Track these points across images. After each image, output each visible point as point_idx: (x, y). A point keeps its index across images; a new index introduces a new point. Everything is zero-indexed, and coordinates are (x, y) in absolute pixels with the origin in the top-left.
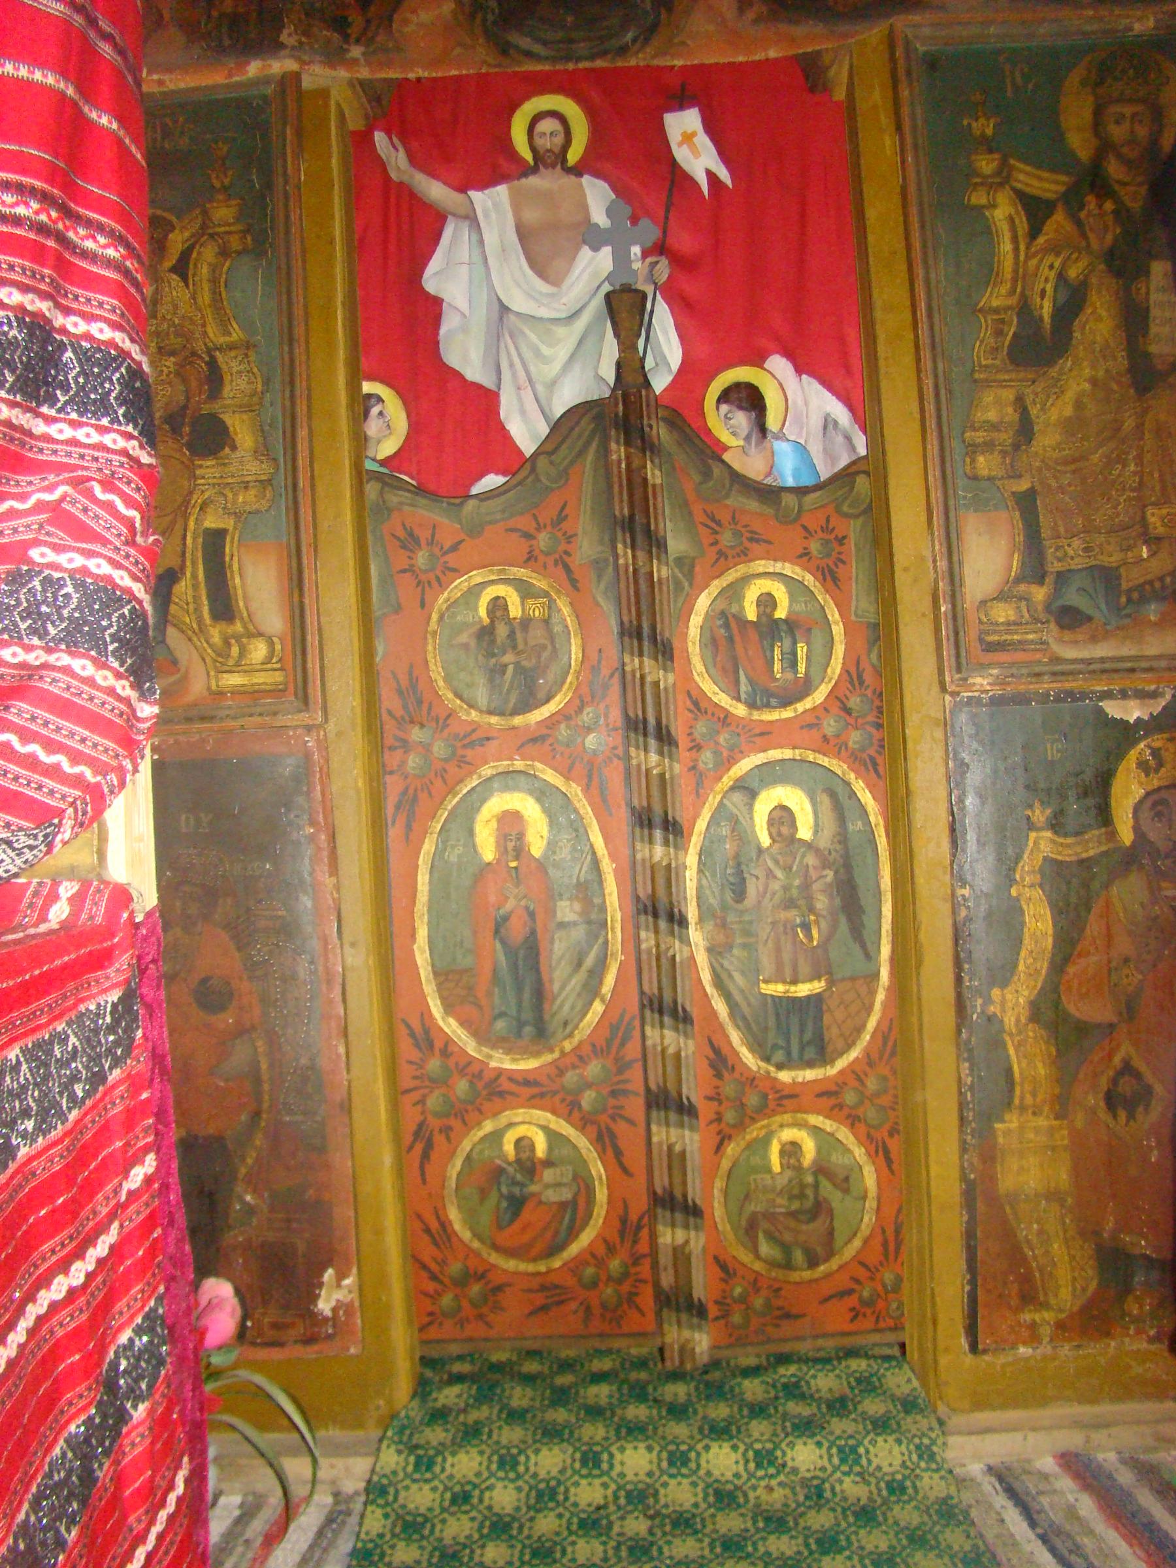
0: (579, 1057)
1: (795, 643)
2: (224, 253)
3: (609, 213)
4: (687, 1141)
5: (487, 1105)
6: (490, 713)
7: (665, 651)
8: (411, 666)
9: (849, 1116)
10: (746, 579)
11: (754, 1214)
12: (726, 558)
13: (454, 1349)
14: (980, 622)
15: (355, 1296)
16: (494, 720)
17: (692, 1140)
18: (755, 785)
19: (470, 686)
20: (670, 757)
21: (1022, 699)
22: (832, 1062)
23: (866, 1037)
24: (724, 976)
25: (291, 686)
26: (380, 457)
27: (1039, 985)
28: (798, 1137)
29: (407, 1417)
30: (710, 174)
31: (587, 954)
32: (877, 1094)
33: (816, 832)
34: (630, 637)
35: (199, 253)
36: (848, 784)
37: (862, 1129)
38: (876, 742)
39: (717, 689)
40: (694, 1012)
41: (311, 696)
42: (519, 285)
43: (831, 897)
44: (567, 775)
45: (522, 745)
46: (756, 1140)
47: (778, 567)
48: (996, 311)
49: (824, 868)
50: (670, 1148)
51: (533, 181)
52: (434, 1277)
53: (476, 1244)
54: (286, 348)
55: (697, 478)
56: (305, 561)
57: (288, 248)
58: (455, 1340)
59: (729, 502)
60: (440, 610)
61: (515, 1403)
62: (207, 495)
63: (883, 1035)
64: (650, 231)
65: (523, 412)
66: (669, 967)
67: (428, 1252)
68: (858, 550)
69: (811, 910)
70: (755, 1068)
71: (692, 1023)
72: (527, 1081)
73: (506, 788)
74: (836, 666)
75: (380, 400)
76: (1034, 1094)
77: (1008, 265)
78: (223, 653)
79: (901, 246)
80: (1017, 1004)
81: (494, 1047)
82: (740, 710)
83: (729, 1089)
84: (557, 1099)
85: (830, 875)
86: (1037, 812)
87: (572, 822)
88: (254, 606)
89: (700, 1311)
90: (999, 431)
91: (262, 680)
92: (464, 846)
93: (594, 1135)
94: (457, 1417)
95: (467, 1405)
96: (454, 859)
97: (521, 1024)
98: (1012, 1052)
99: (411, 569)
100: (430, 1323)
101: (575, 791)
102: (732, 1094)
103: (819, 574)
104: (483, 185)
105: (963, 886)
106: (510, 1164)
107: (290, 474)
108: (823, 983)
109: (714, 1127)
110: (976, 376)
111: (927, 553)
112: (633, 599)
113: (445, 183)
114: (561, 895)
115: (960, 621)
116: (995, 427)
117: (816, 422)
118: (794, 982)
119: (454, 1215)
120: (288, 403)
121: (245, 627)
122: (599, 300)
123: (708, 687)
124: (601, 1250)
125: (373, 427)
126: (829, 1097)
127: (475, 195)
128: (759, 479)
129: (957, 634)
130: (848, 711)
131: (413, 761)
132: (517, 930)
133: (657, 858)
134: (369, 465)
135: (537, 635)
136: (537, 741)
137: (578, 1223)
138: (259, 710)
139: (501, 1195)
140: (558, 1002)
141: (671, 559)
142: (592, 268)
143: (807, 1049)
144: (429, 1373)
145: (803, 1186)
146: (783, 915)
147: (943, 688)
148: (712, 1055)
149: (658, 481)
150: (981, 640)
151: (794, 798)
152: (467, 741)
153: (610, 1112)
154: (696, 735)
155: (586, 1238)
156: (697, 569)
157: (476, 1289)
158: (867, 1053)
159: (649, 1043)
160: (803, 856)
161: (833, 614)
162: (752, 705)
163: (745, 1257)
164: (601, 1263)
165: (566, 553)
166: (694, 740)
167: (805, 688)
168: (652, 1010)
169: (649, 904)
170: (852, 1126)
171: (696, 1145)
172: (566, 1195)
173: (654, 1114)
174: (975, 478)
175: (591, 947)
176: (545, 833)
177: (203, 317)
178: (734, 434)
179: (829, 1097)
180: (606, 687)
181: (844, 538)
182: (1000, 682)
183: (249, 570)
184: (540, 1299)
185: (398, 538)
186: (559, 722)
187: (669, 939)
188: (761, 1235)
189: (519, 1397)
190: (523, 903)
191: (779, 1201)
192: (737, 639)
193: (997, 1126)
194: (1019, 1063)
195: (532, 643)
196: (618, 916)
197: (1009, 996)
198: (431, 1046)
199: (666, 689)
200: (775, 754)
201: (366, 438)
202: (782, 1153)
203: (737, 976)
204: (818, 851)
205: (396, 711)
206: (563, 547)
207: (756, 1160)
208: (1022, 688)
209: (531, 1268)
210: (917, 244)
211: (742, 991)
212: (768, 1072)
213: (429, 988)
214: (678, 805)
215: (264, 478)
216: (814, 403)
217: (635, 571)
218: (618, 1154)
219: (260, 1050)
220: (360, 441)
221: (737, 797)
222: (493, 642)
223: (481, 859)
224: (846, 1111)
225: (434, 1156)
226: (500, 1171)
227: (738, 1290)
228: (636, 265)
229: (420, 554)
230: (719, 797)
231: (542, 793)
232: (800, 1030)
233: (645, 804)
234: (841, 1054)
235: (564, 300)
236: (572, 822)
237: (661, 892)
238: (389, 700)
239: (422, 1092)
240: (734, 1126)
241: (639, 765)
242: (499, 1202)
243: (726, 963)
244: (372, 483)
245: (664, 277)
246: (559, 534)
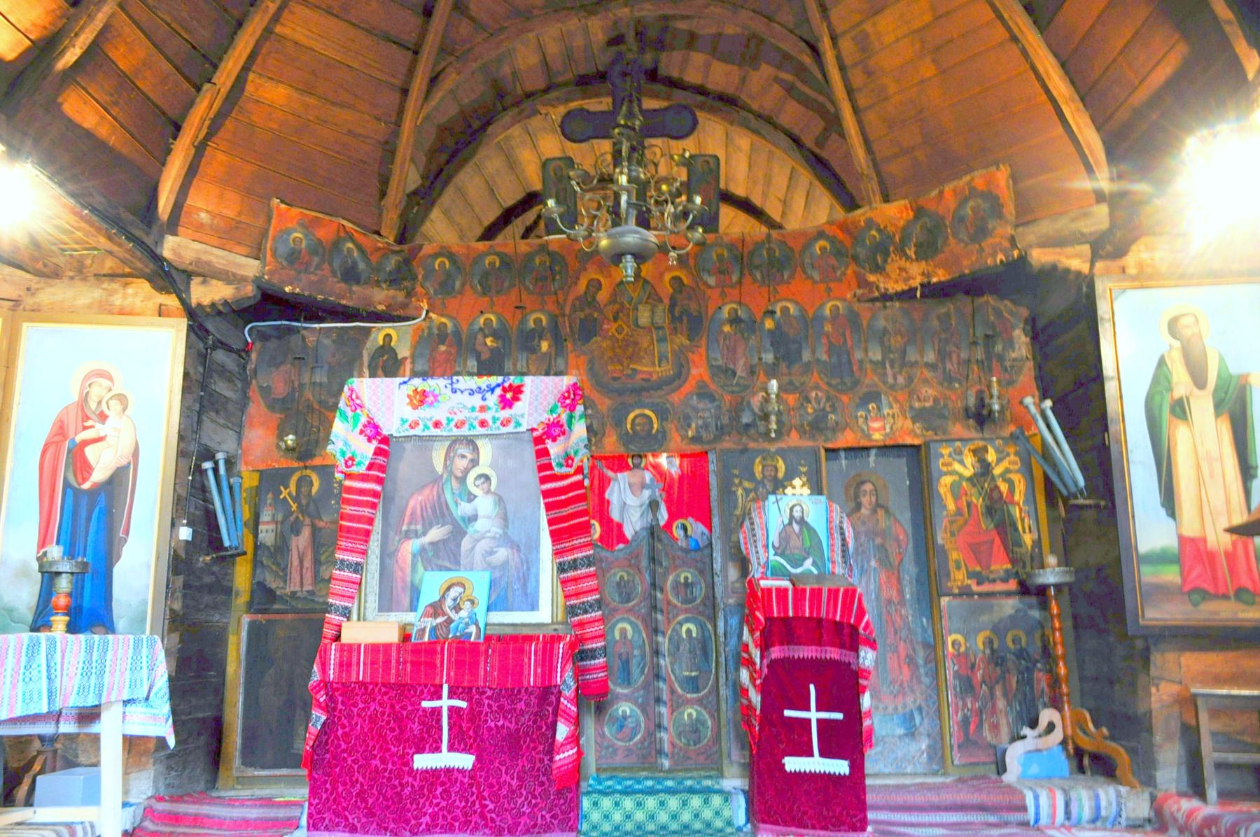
67: (599, 740)
72: (626, 695)
101: (639, 623)
126: (700, 702)
132: (624, 657)
136: (630, 610)
155: (639, 737)
163: (677, 741)
167: (694, 600)
231: (631, 623)
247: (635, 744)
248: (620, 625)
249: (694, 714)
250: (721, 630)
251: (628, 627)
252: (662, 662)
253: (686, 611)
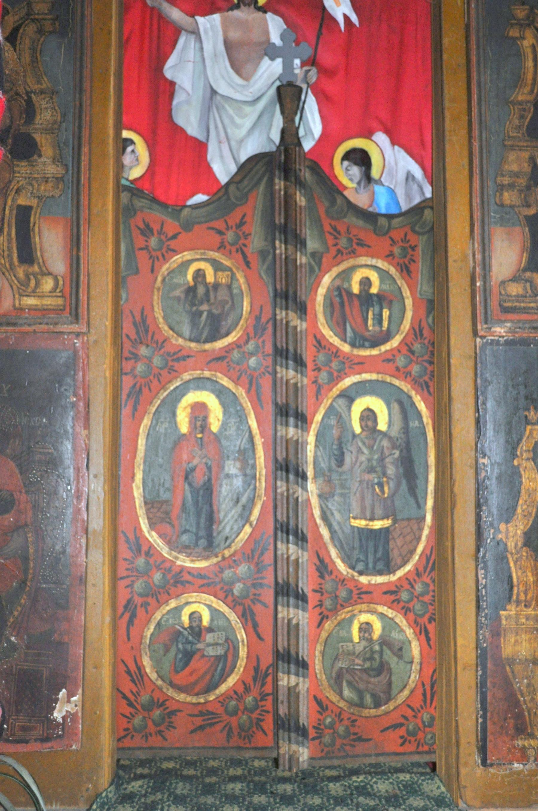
0: (232, 562)
2: (40, 31)
3: (282, 37)
4: (300, 618)
5: (172, 590)
6: (191, 340)
7: (302, 309)
8: (143, 309)
10: (354, 268)
12: (342, 254)
13: (142, 755)
14: (501, 294)
15: (79, 708)
16: (193, 345)
17: (303, 617)
18: (353, 394)
19: (178, 323)
20: (302, 374)
21: (524, 342)
23: (416, 557)
24: (328, 513)
25: (68, 309)
26: (131, 178)
27: (531, 522)
28: (370, 620)
29: (107, 796)
30: (346, 17)
31: (243, 495)
32: (422, 594)
34: (281, 298)
35: (24, 30)
36: (410, 397)
38: (428, 372)
39: (331, 333)
40: (309, 536)
41: (80, 314)
42: (223, 77)
43: (397, 468)
44: (236, 382)
45: (210, 362)
46: (343, 620)
47: (374, 262)
48: (520, 103)
50: (289, 621)
51: (236, 13)
52: (130, 704)
53: (159, 682)
54: (77, 95)
55: (327, 204)
56: (82, 229)
57: (82, 32)
58: (140, 748)
59: (346, 220)
60: (163, 275)
61: (179, 792)
62: (21, 183)
63: (426, 557)
64: (307, 50)
65: (222, 157)
66: (294, 505)
67: (127, 687)
68: (423, 254)
69: (384, 474)
70: (345, 573)
71: (307, 542)
72: (200, 574)
73: (198, 388)
74: (407, 325)
75: (132, 142)
76: (526, 594)
77: (530, 76)
78: (25, 283)
79: (463, 61)
80: (516, 534)
81: (180, 552)
82: (346, 348)
83: (328, 586)
85: (397, 453)
86: (532, 413)
87: (237, 411)
88: (47, 255)
89: (303, 732)
90: (518, 177)
91: (49, 303)
92: (170, 422)
93: (240, 614)
94: (139, 799)
95: (146, 792)
98: (512, 565)
99: (146, 248)
100: (125, 736)
101: (241, 392)
102: (329, 589)
103: (399, 268)
104: (205, 13)
105: (484, 457)
107: (75, 175)
108: (390, 521)
109: (318, 610)
110: (506, 143)
111: (470, 252)
112: (284, 275)
113: (182, 11)
115: (488, 292)
116: (516, 175)
117: (401, 176)
118: (372, 519)
119: (146, 662)
120: (76, 130)
121: (40, 268)
122: (273, 91)
124: (241, 689)
125: (127, 159)
126: (391, 595)
127: (200, 19)
128: (365, 207)
129: (486, 300)
130: (412, 352)
131: (140, 368)
132: (199, 479)
133: (290, 435)
134: (123, 182)
135: (222, 294)
136: (220, 359)
137: (227, 669)
138: (46, 320)
139: (178, 650)
140: (223, 524)
141: (309, 251)
142: (269, 71)
143: (378, 564)
144: (121, 773)
145: (373, 652)
146: (367, 477)
147: (475, 333)
148: (318, 563)
149: (303, 203)
150: (500, 305)
151: (377, 405)
152: (175, 357)
153: (252, 597)
155: (231, 681)
156: (324, 260)
159: (279, 552)
160: (381, 440)
161: (406, 293)
162: (353, 345)
163: (334, 698)
164: (240, 699)
165: (245, 245)
166: (316, 365)
167: (387, 337)
168: (282, 531)
169: (284, 464)
171: (306, 621)
172: (220, 651)
173: (280, 599)
174: (502, 205)
175: (245, 491)
177: (24, 71)
178: (351, 180)
179: (391, 595)
180: (264, 329)
181: (416, 246)
182: (511, 331)
183: (46, 233)
184: (199, 721)
186: (233, 349)
187: (296, 486)
189: (181, 788)
190: (204, 460)
191: (357, 661)
192: (346, 303)
193: (502, 613)
196: (264, 472)
197: (511, 529)
198: (139, 551)
199: (301, 331)
200: (366, 376)
201: (123, 166)
202: (360, 629)
204: (390, 438)
205: (133, 334)
207: (343, 633)
208: (525, 335)
209: (194, 700)
210: (474, 59)
211: (339, 524)
212: (353, 576)
213: (141, 512)
214: (305, 404)
215: (59, 176)
216: (401, 163)
217: (286, 258)
218: (255, 626)
219: (30, 540)
220: (120, 167)
222: (195, 296)
223: (180, 431)
224: (402, 604)
225: (136, 621)
226: (180, 633)
228: (297, 71)
230: (330, 401)
231: (221, 393)
232: (375, 550)
233: (284, 401)
234: (399, 568)
235: (251, 90)
236: (237, 411)
237: (292, 457)
238: (128, 328)
239: (132, 579)
240: (330, 610)
241: (282, 378)
242: (176, 655)
244: (125, 193)
245: (314, 79)
246: (240, 233)
248: (192, 397)
249: (377, 627)
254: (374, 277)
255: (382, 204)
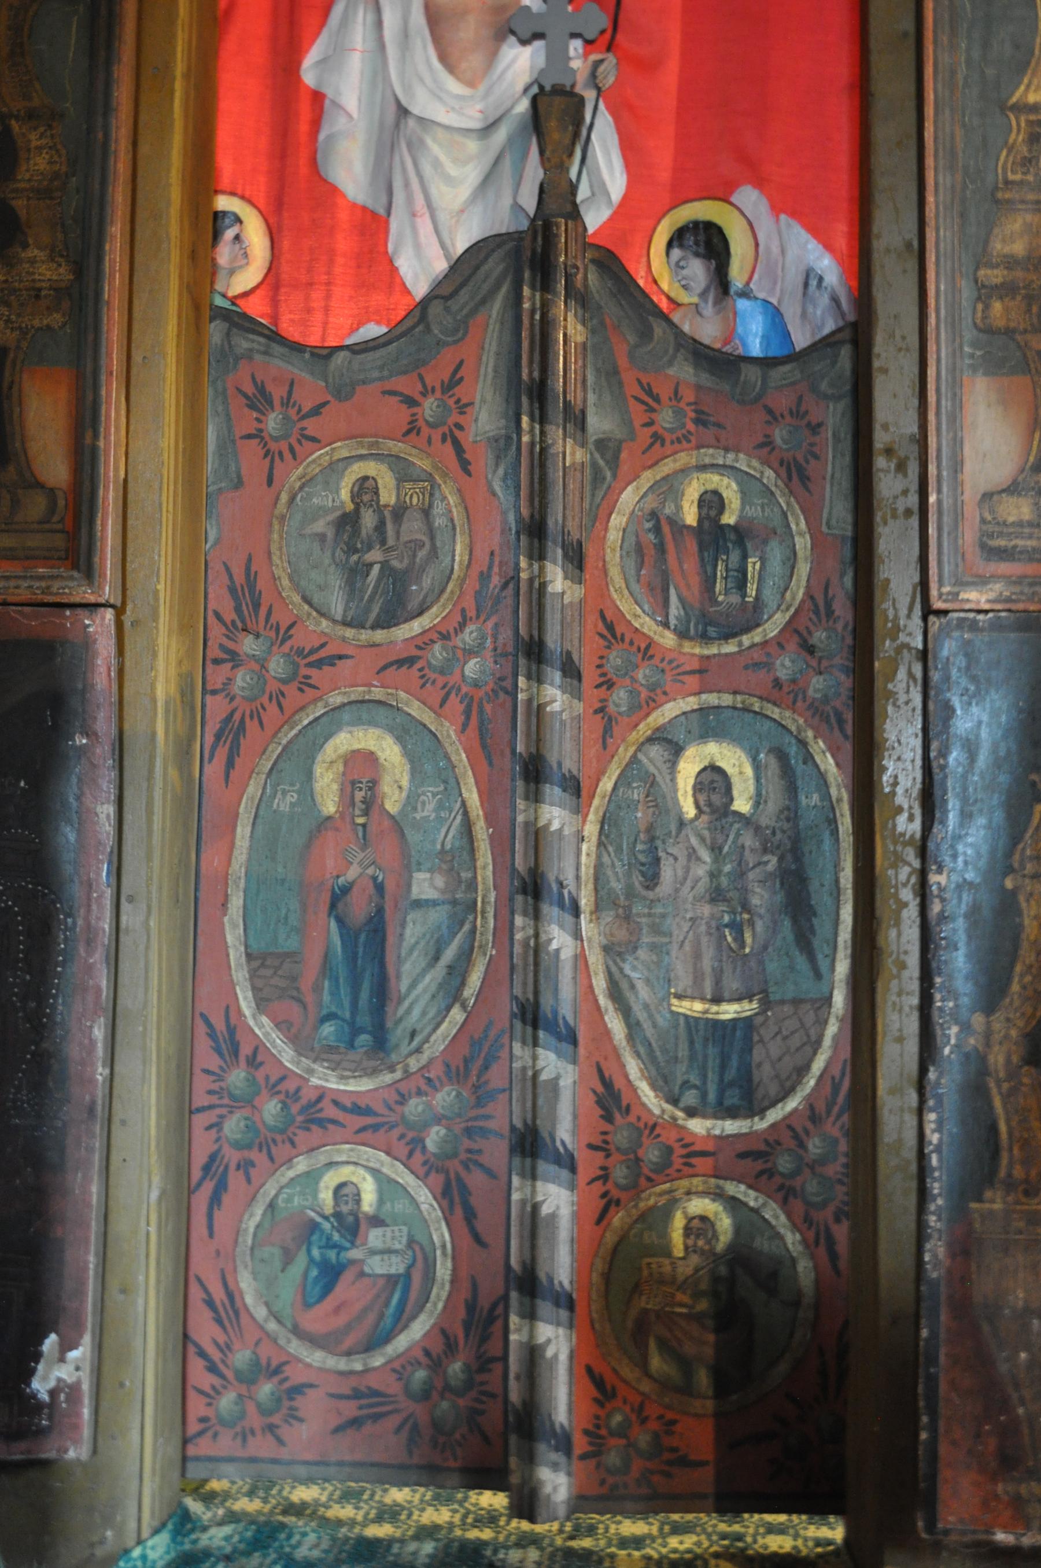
1: (745, 557)
5: (301, 1137)
9: (781, 1187)
11: (645, 1312)
16: (349, 633)
18: (680, 737)
22: (762, 1112)
24: (624, 985)
26: (230, 294)
33: (757, 804)
36: (803, 743)
37: (798, 1206)
44: (439, 708)
45: (384, 668)
49: (765, 851)
53: (272, 1326)
55: (632, 339)
59: (671, 371)
69: (746, 907)
70: (657, 1111)
73: (358, 722)
74: (798, 591)
75: (238, 220)
82: (668, 639)
83: (621, 1138)
84: (396, 1133)
85: (772, 862)
92: (299, 792)
93: (439, 1190)
96: (284, 808)
97: (356, 1030)
99: (258, 435)
101: (448, 732)
106: (326, 1218)
108: (755, 1005)
109: (598, 1188)
114: (419, 864)
117: (793, 278)
118: (717, 1000)
119: (246, 1284)
123: (626, 606)
125: (224, 254)
130: (810, 650)
132: (359, 908)
135: (413, 527)
137: (409, 1308)
139: (312, 1260)
140: (406, 1004)
148: (600, 1089)
151: (732, 759)
153: (463, 1156)
154: (608, 668)
155: (418, 1329)
156: (624, 455)
157: (266, 1389)
158: (810, 1103)
160: (738, 835)
161: (799, 524)
162: (683, 634)
165: (459, 426)
167: (750, 617)
170: (784, 1203)
172: (396, 1266)
176: (405, 782)
178: (685, 287)
185: (246, 396)
186: (433, 642)
188: (652, 1344)
190: (370, 871)
191: (680, 1297)
192: (670, 546)
194: (1008, 1121)
195: (404, 538)
197: (997, 1026)
198: (235, 1053)
202: (688, 1231)
203: (640, 985)
204: (758, 829)
206: (454, 418)
209: (342, 1364)
212: (674, 1119)
218: (470, 1216)
221: (655, 751)
222: (356, 532)
224: (778, 1180)
226: (313, 1227)
227: (618, 1418)
229: (272, 416)
231: (405, 731)
234: (773, 1104)
239: (218, 1111)
240: (624, 1188)
243: (627, 970)
246: (451, 402)
247: (400, 1368)
249: (725, 1223)
250: (900, 772)
251: (389, 751)
252: (559, 939)
253: (704, 673)
254: (730, 490)
255: (754, 340)
